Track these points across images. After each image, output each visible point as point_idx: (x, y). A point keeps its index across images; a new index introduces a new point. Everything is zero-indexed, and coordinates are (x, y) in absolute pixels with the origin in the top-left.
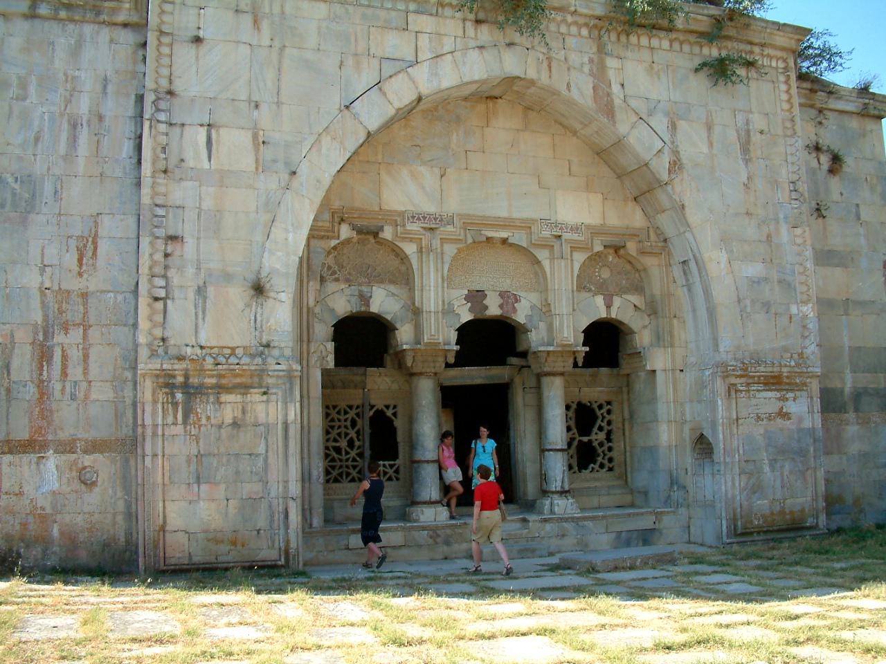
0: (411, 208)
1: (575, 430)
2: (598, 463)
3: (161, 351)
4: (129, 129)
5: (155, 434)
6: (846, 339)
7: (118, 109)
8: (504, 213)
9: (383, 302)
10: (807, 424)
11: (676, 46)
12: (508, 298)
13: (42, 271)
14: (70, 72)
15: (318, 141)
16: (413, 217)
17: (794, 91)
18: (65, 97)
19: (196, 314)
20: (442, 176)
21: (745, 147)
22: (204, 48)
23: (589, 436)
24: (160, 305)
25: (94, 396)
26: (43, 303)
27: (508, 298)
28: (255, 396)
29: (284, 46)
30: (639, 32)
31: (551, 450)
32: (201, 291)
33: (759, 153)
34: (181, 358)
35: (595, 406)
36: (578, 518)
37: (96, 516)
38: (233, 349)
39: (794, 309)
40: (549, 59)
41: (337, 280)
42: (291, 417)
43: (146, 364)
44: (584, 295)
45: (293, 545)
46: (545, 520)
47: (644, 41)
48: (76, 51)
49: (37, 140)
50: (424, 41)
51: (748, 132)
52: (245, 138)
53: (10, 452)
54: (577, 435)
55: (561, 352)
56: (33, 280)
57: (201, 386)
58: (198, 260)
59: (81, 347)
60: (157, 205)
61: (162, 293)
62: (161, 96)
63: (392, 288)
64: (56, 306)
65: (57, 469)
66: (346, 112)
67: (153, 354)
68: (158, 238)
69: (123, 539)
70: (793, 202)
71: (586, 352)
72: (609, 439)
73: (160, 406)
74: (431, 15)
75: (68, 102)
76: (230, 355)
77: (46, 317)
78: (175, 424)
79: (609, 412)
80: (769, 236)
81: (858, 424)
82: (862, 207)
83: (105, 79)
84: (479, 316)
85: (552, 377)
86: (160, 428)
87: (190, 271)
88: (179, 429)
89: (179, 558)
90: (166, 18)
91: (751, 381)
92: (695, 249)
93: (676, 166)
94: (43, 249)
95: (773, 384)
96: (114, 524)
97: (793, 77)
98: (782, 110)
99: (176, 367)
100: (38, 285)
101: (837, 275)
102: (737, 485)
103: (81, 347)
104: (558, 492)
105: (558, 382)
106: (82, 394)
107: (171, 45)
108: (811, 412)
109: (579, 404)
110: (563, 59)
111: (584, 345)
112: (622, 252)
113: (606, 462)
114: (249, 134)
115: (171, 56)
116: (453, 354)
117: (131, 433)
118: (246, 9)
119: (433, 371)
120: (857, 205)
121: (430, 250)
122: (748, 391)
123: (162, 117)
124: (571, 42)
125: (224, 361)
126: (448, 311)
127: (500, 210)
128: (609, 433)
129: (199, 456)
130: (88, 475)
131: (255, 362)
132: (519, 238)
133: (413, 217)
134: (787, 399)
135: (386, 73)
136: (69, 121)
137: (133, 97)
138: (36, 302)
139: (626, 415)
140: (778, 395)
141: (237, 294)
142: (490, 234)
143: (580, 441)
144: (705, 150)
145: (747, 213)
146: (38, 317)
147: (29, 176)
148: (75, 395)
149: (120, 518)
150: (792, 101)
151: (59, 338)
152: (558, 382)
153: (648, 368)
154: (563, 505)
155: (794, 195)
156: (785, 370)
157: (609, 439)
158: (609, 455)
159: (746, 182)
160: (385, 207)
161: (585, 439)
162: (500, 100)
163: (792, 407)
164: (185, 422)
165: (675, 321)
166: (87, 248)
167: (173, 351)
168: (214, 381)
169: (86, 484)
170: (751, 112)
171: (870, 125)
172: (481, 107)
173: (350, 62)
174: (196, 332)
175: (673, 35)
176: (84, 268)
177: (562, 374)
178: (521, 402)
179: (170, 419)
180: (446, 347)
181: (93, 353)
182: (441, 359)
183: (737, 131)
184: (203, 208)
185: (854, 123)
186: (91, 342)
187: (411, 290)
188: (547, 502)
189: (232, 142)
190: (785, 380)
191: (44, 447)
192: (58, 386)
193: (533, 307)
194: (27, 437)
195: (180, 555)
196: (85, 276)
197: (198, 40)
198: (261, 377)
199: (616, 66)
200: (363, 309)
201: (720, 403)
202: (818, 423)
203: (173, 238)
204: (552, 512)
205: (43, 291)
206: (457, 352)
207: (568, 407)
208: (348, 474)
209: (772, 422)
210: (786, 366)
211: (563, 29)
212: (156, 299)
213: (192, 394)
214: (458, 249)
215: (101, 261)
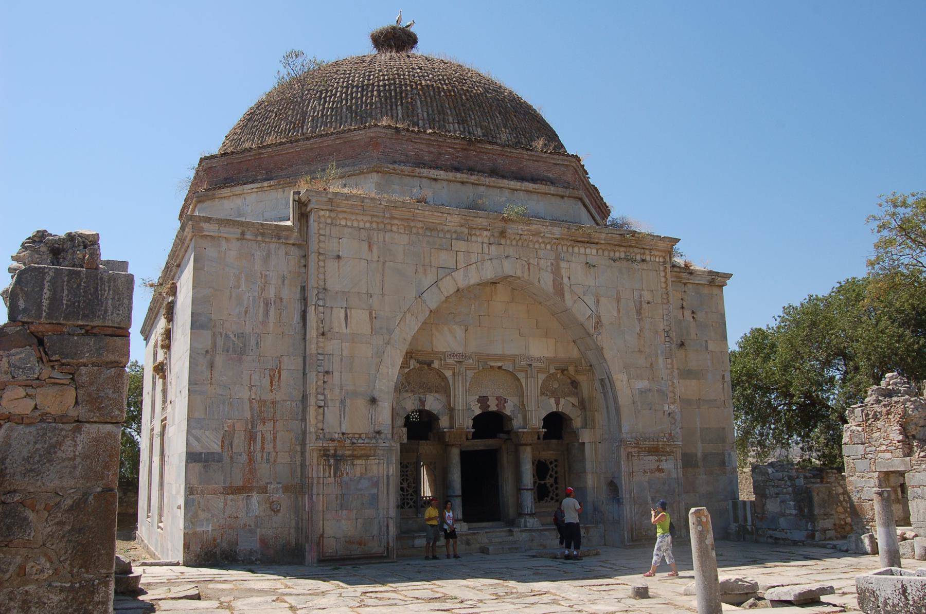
0: (449, 350)
1: (536, 477)
2: (550, 497)
3: (321, 436)
4: (297, 308)
5: (318, 483)
6: (698, 423)
7: (290, 294)
8: (500, 352)
9: (433, 403)
10: (674, 475)
11: (600, 252)
12: (501, 400)
13: (250, 390)
14: (263, 272)
15: (404, 316)
16: (450, 355)
17: (669, 276)
18: (261, 287)
19: (340, 415)
20: (466, 331)
21: (639, 312)
22: (342, 262)
23: (544, 480)
24: (321, 410)
25: (279, 460)
26: (251, 407)
27: (501, 400)
28: (373, 461)
29: (386, 261)
30: (579, 245)
31: (525, 489)
32: (342, 402)
33: (647, 314)
34: (332, 440)
35: (548, 463)
36: (541, 530)
37: (279, 529)
38: (360, 434)
39: (666, 407)
40: (529, 264)
41: (407, 391)
42: (391, 472)
43: (314, 443)
44: (544, 398)
45: (391, 544)
46: (522, 531)
47: (582, 250)
48: (266, 259)
49: (246, 312)
50: (461, 256)
51: (641, 302)
52: (365, 315)
53: (232, 493)
54: (537, 480)
55: (531, 432)
56: (245, 394)
57: (343, 456)
58: (341, 384)
59: (272, 432)
60: (319, 354)
61: (322, 404)
62: (320, 291)
63: (437, 395)
64: (258, 409)
65: (258, 503)
66: (419, 299)
67: (318, 438)
68: (319, 372)
69: (294, 543)
70: (666, 343)
71: (545, 432)
72: (556, 482)
73: (322, 467)
74: (464, 240)
75: (263, 290)
76: (359, 438)
77: (252, 415)
78: (330, 477)
79: (556, 466)
80: (652, 364)
81: (706, 474)
82: (709, 342)
83: (284, 277)
84: (485, 411)
85: (525, 447)
86: (321, 479)
87: (337, 391)
88: (332, 480)
89: (331, 553)
90: (321, 245)
91: (640, 450)
92: (607, 371)
93: (598, 324)
94: (251, 375)
95: (654, 452)
96: (289, 534)
97: (668, 266)
98: (661, 288)
99: (330, 445)
100: (248, 397)
101: (693, 384)
102: (633, 511)
103: (272, 432)
104: (529, 514)
105: (529, 449)
106: (273, 459)
107: (324, 261)
108: (676, 468)
109: (539, 461)
110: (536, 264)
111: (544, 427)
112: (566, 372)
113: (554, 496)
114: (368, 312)
115: (324, 267)
116: (471, 434)
117: (299, 482)
118: (364, 239)
119: (459, 443)
120: (706, 341)
121: (459, 374)
122: (639, 456)
123: (321, 303)
124: (541, 253)
125: (356, 441)
126: (469, 409)
127: (497, 350)
128: (556, 479)
129: (343, 495)
130: (275, 506)
131: (372, 442)
132: (508, 366)
133: (450, 355)
134: (662, 461)
135: (440, 277)
136: (264, 302)
137: (299, 287)
138: (247, 406)
139: (566, 469)
140: (657, 458)
141: (361, 404)
142: (492, 364)
143: (539, 483)
144: (616, 314)
145: (639, 351)
146: (248, 415)
147: (242, 333)
148: (269, 460)
149: (292, 531)
150: (667, 282)
151: (260, 427)
152: (529, 449)
153: (580, 441)
154: (532, 522)
155: (667, 339)
156: (660, 443)
157: (556, 482)
158: (556, 492)
159: (639, 332)
160: (435, 349)
161: (543, 482)
162: (498, 285)
163: (664, 465)
164: (335, 476)
165: (596, 413)
166: (275, 375)
167: (328, 436)
168: (350, 452)
169: (274, 511)
170: (643, 290)
171: (715, 291)
172: (488, 289)
173: (421, 270)
174: (340, 425)
175: (598, 246)
176: (274, 387)
177: (531, 445)
178: (506, 460)
179: (327, 474)
180: (468, 430)
181: (278, 435)
182: (464, 437)
183: (634, 302)
184: (344, 355)
185: (706, 291)
186: (278, 430)
187: (448, 396)
188: (523, 520)
189: (359, 316)
190: (661, 449)
191: (251, 490)
192: (259, 455)
193: (514, 406)
194: (242, 484)
195: (331, 551)
196: (274, 392)
197: (339, 257)
198: (375, 450)
199: (566, 266)
200: (421, 408)
201: (623, 463)
202: (681, 475)
203: (327, 372)
204: (526, 526)
205: (250, 400)
206: (474, 433)
207: (533, 463)
208: (408, 503)
209: (653, 474)
210: (661, 441)
211: (537, 246)
212: (320, 407)
213: (339, 460)
214: (475, 373)
215: (283, 384)
